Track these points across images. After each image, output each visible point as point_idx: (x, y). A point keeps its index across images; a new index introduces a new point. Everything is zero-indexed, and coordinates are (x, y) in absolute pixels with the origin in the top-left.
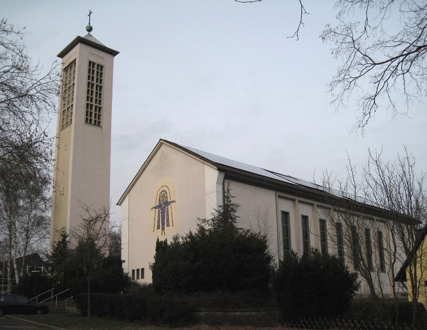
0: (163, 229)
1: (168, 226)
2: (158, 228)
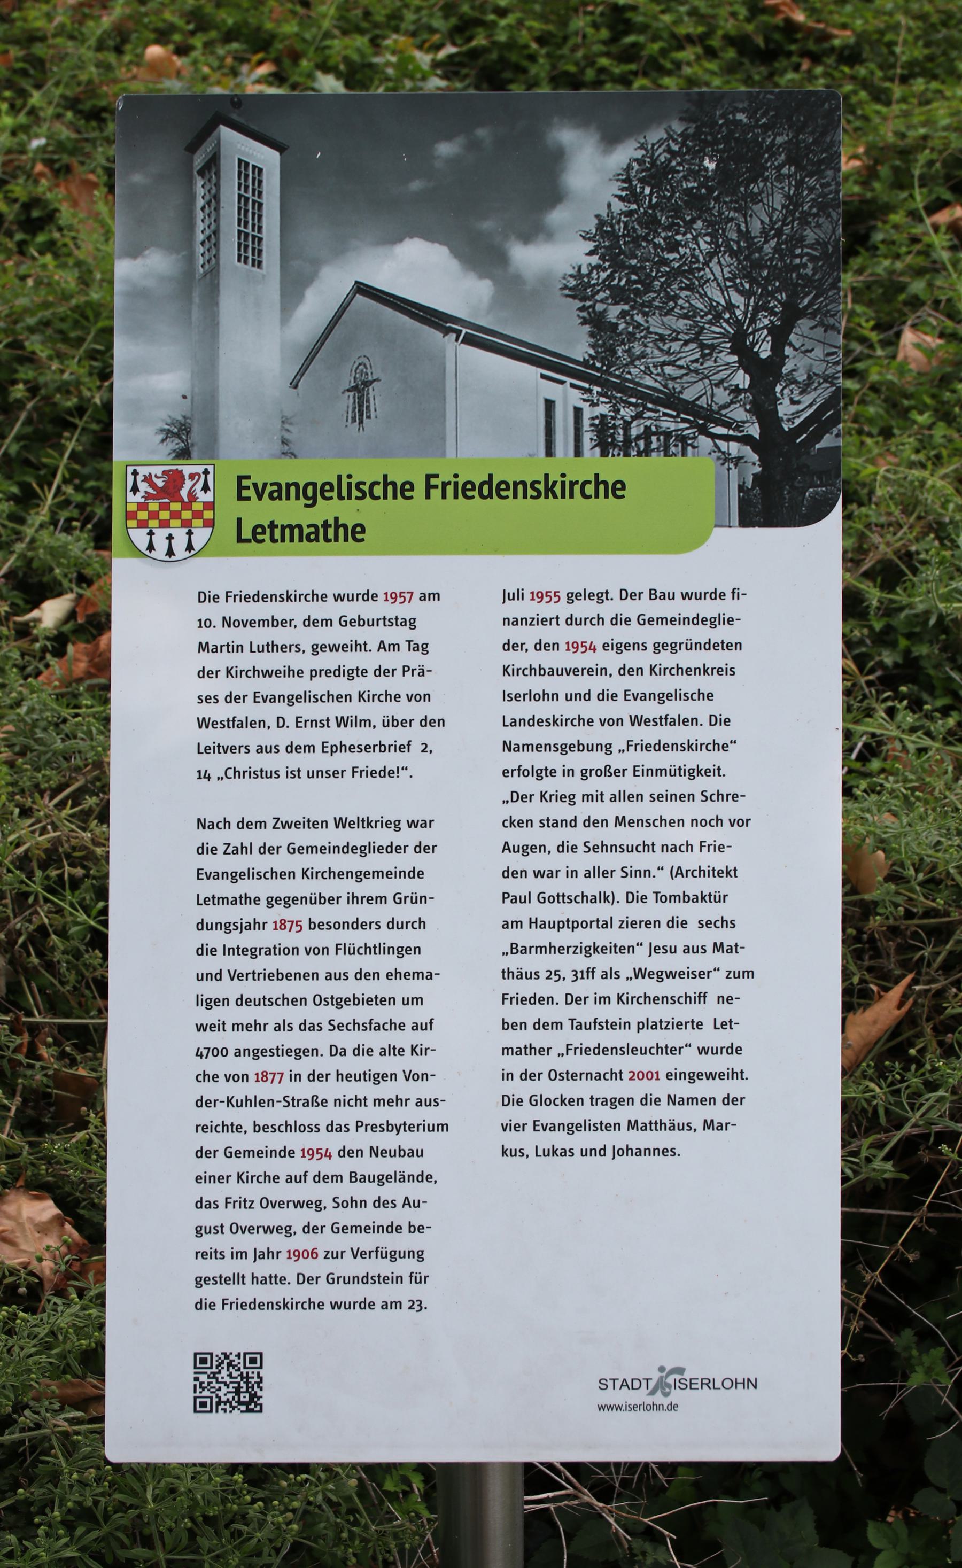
0: (361, 422)
1: (369, 417)
2: (354, 420)
